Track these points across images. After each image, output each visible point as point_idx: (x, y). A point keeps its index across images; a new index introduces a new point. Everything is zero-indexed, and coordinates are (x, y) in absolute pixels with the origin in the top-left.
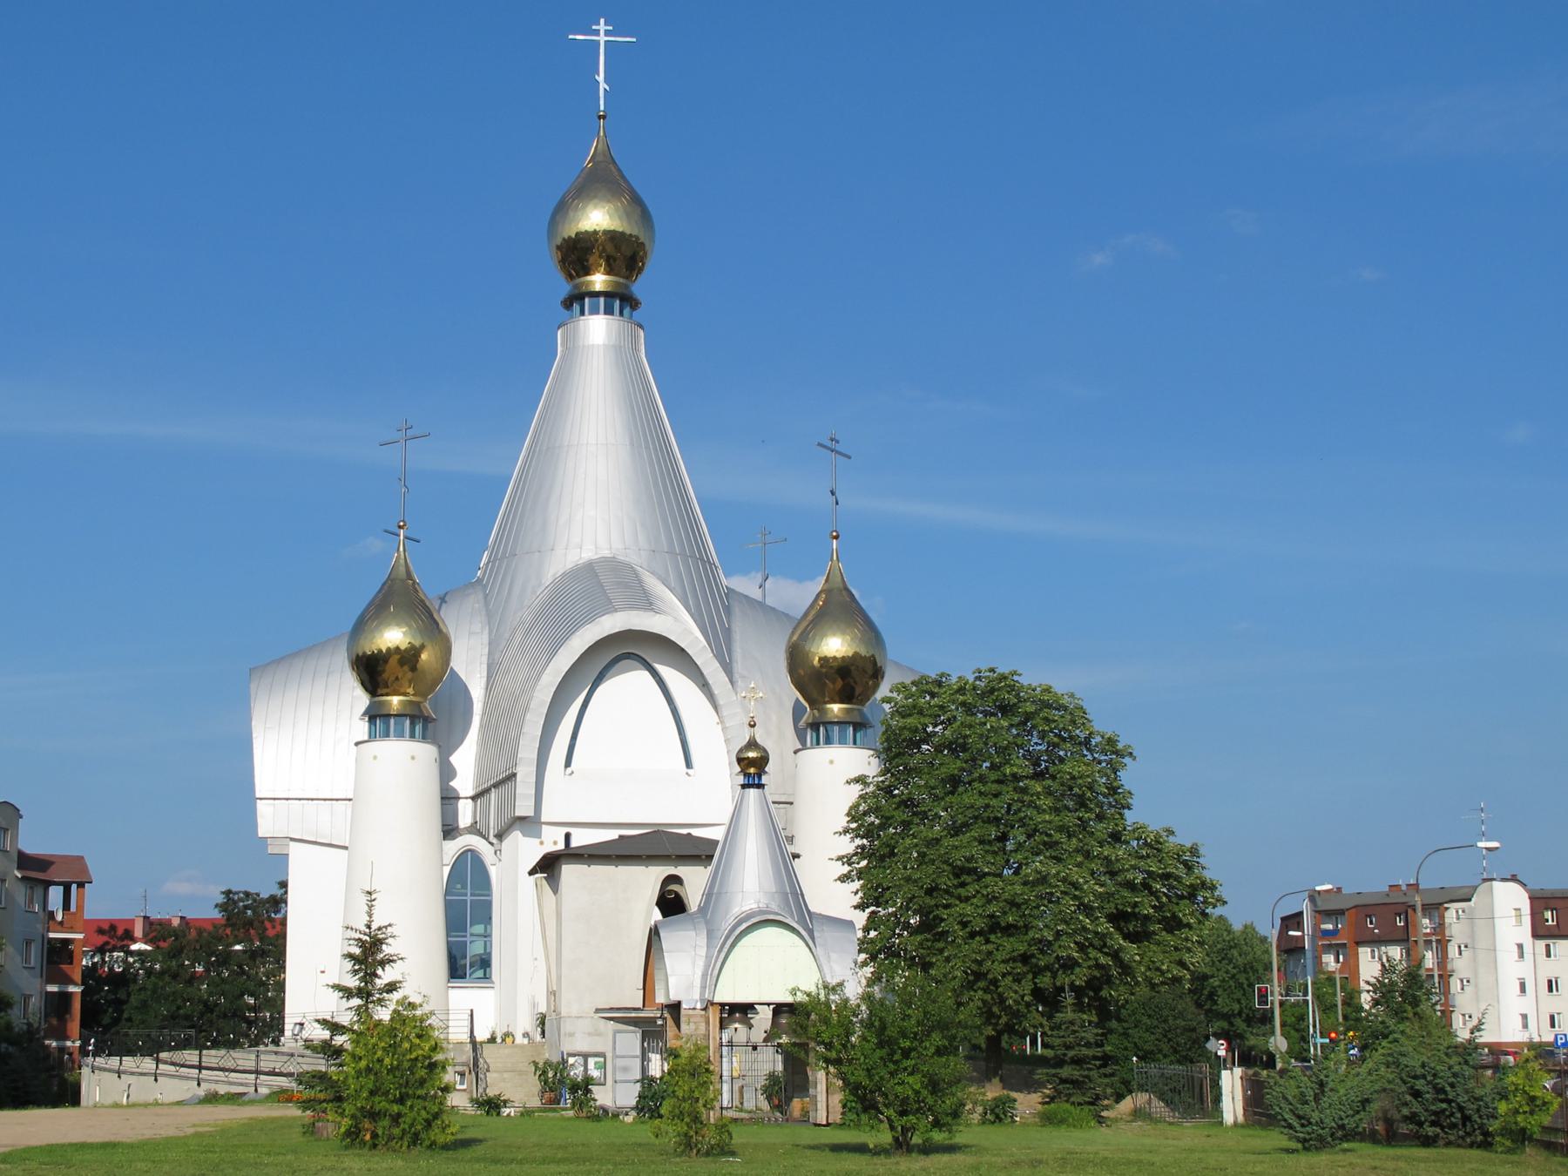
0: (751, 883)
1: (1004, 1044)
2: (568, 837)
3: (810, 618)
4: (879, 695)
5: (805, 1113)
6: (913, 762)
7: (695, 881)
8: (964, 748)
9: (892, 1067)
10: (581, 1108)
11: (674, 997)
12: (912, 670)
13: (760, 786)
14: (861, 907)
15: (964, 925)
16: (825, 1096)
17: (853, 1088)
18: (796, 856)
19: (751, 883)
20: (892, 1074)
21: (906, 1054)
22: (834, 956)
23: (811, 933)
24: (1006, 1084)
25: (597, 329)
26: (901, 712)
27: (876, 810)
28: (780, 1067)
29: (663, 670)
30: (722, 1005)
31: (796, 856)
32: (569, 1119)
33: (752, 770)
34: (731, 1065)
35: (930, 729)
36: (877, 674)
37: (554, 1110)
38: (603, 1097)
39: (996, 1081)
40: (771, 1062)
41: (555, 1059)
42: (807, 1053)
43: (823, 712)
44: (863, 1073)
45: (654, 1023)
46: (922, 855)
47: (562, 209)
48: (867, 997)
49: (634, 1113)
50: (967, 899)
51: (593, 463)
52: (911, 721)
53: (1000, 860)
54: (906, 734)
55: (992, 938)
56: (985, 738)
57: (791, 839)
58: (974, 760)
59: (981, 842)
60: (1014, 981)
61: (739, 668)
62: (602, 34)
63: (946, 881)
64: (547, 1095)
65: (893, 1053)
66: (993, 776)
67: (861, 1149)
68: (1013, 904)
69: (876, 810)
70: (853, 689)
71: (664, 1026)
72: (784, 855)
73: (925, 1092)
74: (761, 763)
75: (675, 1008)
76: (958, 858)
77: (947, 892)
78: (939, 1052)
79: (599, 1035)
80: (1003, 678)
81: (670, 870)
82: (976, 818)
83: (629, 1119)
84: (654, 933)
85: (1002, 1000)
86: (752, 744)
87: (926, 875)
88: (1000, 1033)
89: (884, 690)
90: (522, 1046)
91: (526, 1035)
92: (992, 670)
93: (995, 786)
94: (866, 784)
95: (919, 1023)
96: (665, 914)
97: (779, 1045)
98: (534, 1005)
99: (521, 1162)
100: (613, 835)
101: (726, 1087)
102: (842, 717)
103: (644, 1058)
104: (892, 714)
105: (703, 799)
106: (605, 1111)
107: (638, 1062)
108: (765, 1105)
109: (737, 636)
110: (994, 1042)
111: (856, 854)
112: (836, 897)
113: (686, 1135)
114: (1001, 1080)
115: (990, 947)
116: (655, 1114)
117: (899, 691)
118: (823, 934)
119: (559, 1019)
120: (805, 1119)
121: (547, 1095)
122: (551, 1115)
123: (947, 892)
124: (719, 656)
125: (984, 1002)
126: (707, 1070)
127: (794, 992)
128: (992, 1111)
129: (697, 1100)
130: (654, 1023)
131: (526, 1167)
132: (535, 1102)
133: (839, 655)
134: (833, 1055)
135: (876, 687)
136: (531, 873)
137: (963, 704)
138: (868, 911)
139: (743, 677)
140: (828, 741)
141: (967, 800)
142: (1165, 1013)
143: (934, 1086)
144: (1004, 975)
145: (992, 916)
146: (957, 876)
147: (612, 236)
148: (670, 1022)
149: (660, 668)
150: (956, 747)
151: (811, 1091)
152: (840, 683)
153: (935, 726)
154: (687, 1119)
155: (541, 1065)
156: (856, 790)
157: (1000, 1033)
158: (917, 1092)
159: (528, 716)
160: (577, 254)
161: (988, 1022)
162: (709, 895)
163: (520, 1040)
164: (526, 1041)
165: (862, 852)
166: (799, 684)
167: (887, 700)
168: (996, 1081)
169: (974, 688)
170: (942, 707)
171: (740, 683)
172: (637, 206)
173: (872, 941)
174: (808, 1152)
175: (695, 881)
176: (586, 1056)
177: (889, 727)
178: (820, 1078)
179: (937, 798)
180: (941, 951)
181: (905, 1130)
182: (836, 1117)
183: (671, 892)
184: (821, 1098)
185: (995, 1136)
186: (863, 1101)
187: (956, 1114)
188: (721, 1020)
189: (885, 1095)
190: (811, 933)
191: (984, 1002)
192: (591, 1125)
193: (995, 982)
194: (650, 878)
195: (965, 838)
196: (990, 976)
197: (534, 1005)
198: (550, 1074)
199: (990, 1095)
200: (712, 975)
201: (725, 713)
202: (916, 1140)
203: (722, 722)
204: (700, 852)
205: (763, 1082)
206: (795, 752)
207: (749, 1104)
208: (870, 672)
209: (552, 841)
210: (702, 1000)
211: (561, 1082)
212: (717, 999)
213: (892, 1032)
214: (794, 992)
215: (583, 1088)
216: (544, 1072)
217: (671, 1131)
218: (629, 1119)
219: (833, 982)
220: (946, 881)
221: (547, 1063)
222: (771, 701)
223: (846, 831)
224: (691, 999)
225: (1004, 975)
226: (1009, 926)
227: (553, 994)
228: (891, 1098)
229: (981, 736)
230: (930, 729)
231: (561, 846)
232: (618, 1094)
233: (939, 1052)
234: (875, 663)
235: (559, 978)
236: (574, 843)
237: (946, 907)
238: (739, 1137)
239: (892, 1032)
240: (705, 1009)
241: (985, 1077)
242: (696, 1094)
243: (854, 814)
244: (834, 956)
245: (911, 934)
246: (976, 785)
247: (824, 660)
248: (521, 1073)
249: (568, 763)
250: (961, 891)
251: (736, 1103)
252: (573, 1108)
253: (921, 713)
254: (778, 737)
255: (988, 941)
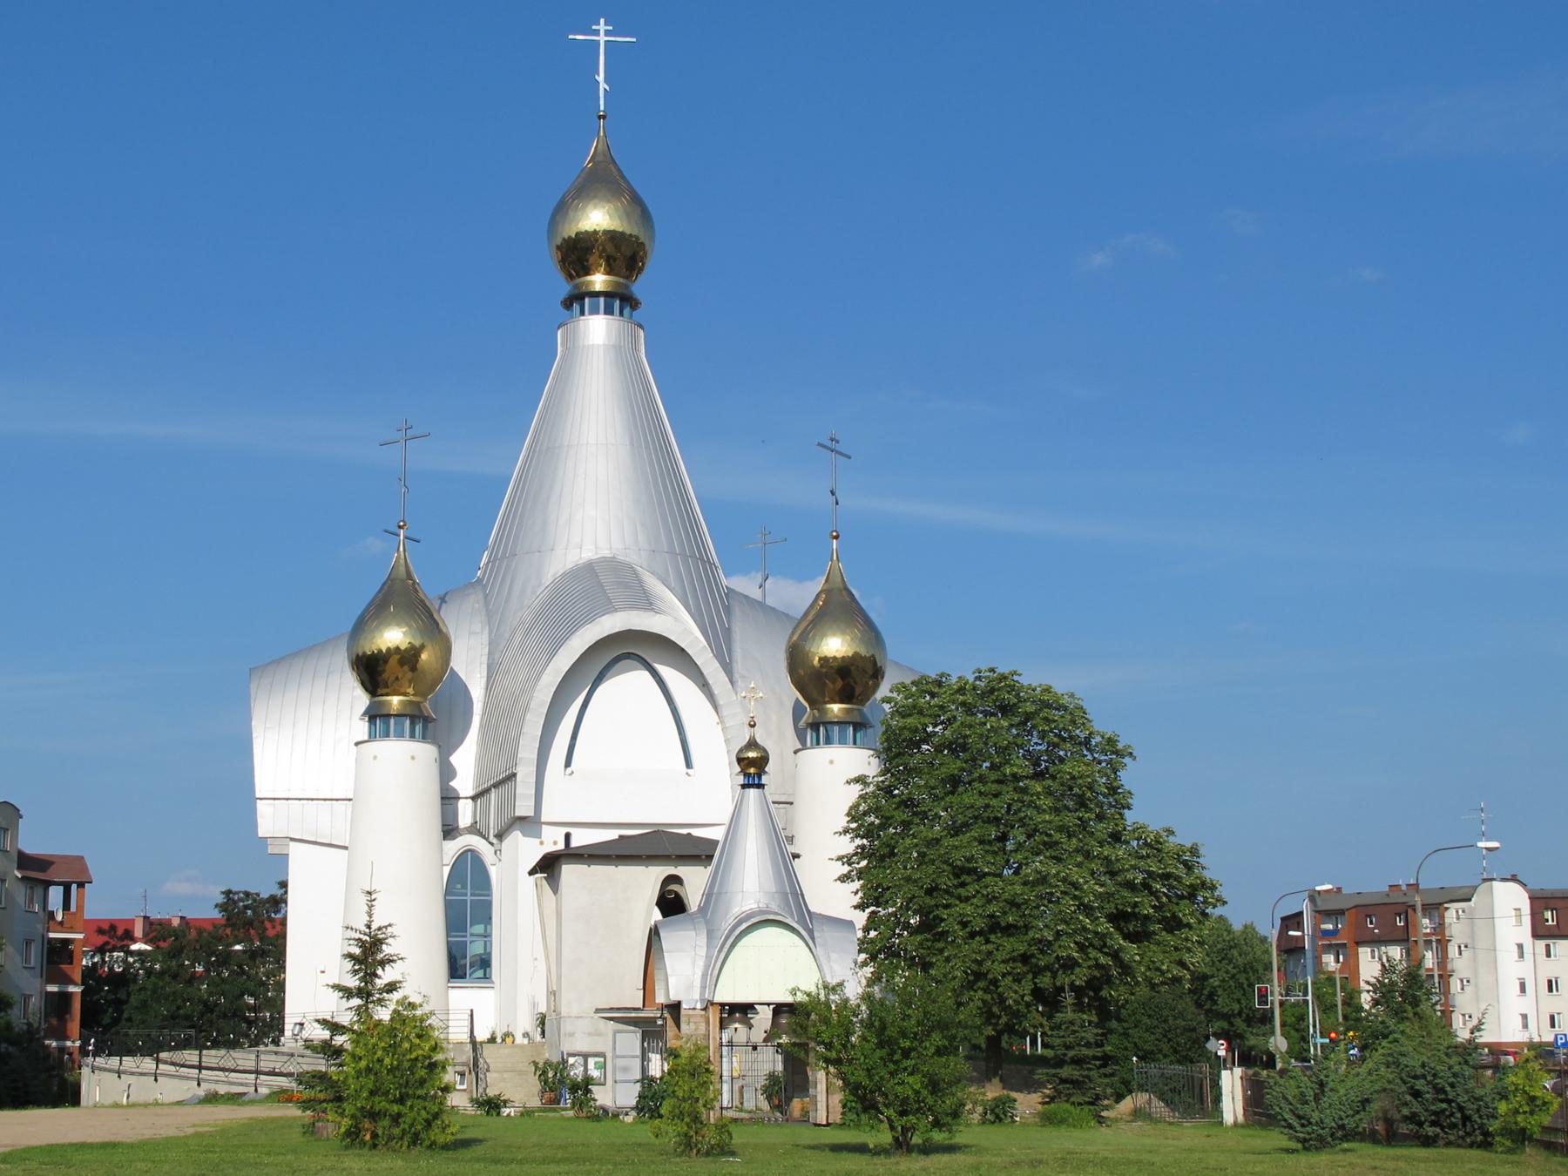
0: (751, 883)
1: (1004, 1044)
2: (568, 837)
3: (810, 618)
4: (879, 695)
5: (805, 1113)
6: (913, 762)
7: (695, 881)
8: (964, 748)
9: (892, 1067)
10: (581, 1108)
11: (674, 997)
12: (912, 670)
13: (760, 786)
14: (861, 907)
15: (964, 925)
16: (825, 1096)
17: (853, 1088)
18: (796, 856)
19: (751, 883)
20: (892, 1074)
21: (906, 1054)
22: (834, 956)
23: (811, 933)
24: (1006, 1084)
25: (597, 329)
26: (901, 712)
27: (876, 810)
28: (780, 1067)
29: (663, 670)
30: (722, 1005)
31: (796, 856)
32: (569, 1119)
33: (752, 770)
34: (731, 1065)
35: (930, 729)
36: (877, 674)
37: (554, 1110)
38: (603, 1097)
39: (996, 1081)
40: (771, 1062)
41: (555, 1059)
42: (807, 1053)
43: (823, 712)
44: (863, 1073)
45: (654, 1023)
46: (922, 855)
47: (562, 209)
48: (867, 997)
49: (634, 1113)
50: (967, 899)
51: (593, 463)
52: (911, 721)
53: (1000, 860)
54: (906, 734)
55: (992, 938)
56: (985, 738)
57: (791, 839)
58: (974, 760)
59: (981, 842)
60: (1014, 981)
61: (739, 668)
62: (602, 34)
63: (946, 881)
64: (547, 1095)
65: (893, 1053)
66: (993, 776)
67: (861, 1149)
68: (1013, 904)
69: (876, 810)
70: (853, 689)
71: (664, 1026)
72: (784, 855)
73: (925, 1092)
74: (761, 763)
75: (675, 1008)
76: (958, 858)
77: (947, 892)
78: (939, 1052)
79: (599, 1035)
80: (1003, 678)
81: (670, 870)
82: (976, 818)
83: (629, 1119)
84: (654, 933)
85: (1002, 1000)
86: (752, 744)
87: (926, 875)
88: (1000, 1033)
89: (884, 690)
90: (522, 1046)
91: (526, 1035)
92: (992, 670)
93: (995, 786)
94: (866, 784)
95: (919, 1023)
96: (665, 914)
97: (779, 1045)
98: (534, 1005)
99: (521, 1162)
100: (613, 835)
101: (726, 1087)
102: (842, 717)
103: (644, 1058)
104: (892, 714)
105: (703, 799)
106: (605, 1111)
107: (638, 1062)
108: (765, 1105)
109: (737, 636)
110: (994, 1042)
111: (856, 854)
112: (836, 897)
113: (686, 1135)
114: (1001, 1080)
115: (990, 947)
116: (655, 1114)
117: (899, 691)
118: (823, 934)
119: (559, 1019)
120: (805, 1119)
121: (547, 1095)
122: (551, 1115)
123: (947, 892)
124: (719, 656)
125: (984, 1002)
126: (707, 1070)
127: (794, 992)
128: (992, 1111)
129: (697, 1100)
130: (654, 1023)
131: (526, 1167)
132: (535, 1102)
133: (839, 655)
134: (833, 1055)
135: (876, 687)
136: (531, 873)
137: (963, 704)
138: (868, 911)
139: (743, 677)
140: (828, 741)
141: (967, 800)
142: (1165, 1013)
143: (934, 1086)
144: (1004, 975)
145: (992, 916)
146: (957, 876)
147: (612, 236)
148: (670, 1022)
149: (660, 668)
150: (956, 747)
151: (811, 1091)
152: (840, 683)
153: (935, 726)
154: (687, 1119)
155: (541, 1065)
156: (856, 790)
157: (1000, 1033)
158: (917, 1092)
159: (528, 716)
160: (577, 254)
161: (988, 1022)
162: (709, 895)
163: (520, 1040)
164: (526, 1041)
165: (862, 852)
166: (799, 684)
167: (887, 700)
168: (996, 1081)
169: (974, 688)
170: (942, 707)
171: (740, 683)
172: (637, 206)
173: (872, 941)
174: (808, 1152)
175: (695, 881)
176: (586, 1056)
177: (889, 727)
178: (820, 1078)
179: (937, 798)
180: (941, 951)
181: (905, 1130)
182: (836, 1117)
183: (671, 892)
184: (821, 1098)
185: (995, 1136)
186: (863, 1101)
187: (956, 1114)
188: (721, 1020)
189: (885, 1095)
190: (811, 933)
191: (984, 1002)
192: (591, 1125)
193: (995, 982)
194: (650, 878)
195: (965, 838)
196: (990, 976)
197: (534, 1005)
198: (550, 1074)
199: (990, 1095)
200: (712, 975)
201: (725, 713)
202: (916, 1140)
203: (722, 722)
204: (700, 852)
205: (763, 1082)
206: (795, 752)
207: (749, 1104)
208: (870, 672)
209: (552, 841)
210: (702, 1000)
211: (561, 1082)
212: (717, 999)
213: (892, 1032)
214: (794, 992)
215: (583, 1088)
216: (544, 1072)
217: (671, 1131)
218: (629, 1119)
219: (833, 982)
220: (946, 881)
221: (547, 1063)
222: (771, 701)
223: (846, 831)
224: (691, 999)
225: (1004, 975)
226: (1009, 926)
227: (553, 994)
228: (891, 1098)
229: (981, 736)
230: (930, 729)
231: (561, 846)
232: (618, 1094)
233: (939, 1052)
234: (875, 663)
235: (559, 978)
236: (574, 843)
237: (946, 907)
238: (739, 1137)
239: (892, 1032)
240: (705, 1009)
241: (985, 1077)
242: (696, 1094)
243: (854, 814)
244: (834, 956)
245: (911, 934)
246: (976, 785)
247: (824, 660)
248: (521, 1073)
249: (568, 763)
250: (961, 891)
251: (736, 1103)
252: (573, 1108)
253: (921, 713)
254: (778, 737)
255: (988, 941)
